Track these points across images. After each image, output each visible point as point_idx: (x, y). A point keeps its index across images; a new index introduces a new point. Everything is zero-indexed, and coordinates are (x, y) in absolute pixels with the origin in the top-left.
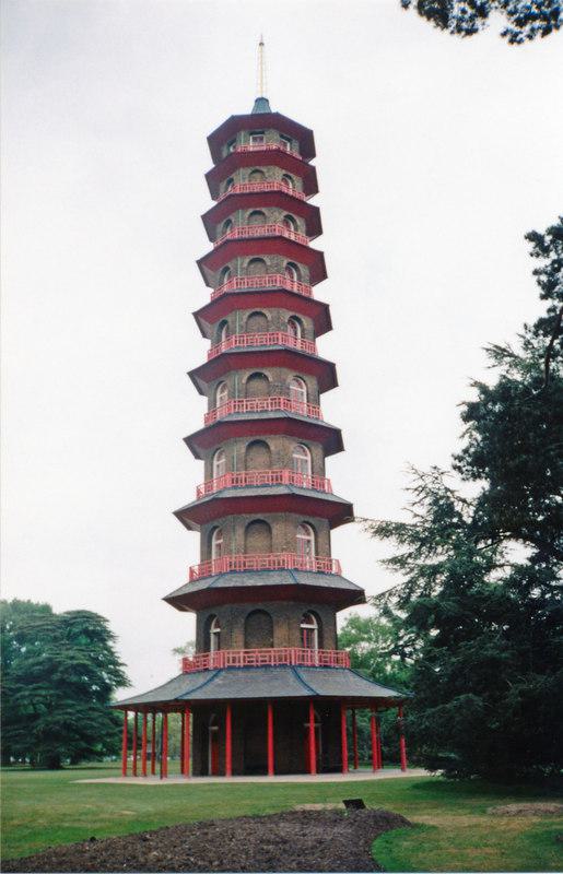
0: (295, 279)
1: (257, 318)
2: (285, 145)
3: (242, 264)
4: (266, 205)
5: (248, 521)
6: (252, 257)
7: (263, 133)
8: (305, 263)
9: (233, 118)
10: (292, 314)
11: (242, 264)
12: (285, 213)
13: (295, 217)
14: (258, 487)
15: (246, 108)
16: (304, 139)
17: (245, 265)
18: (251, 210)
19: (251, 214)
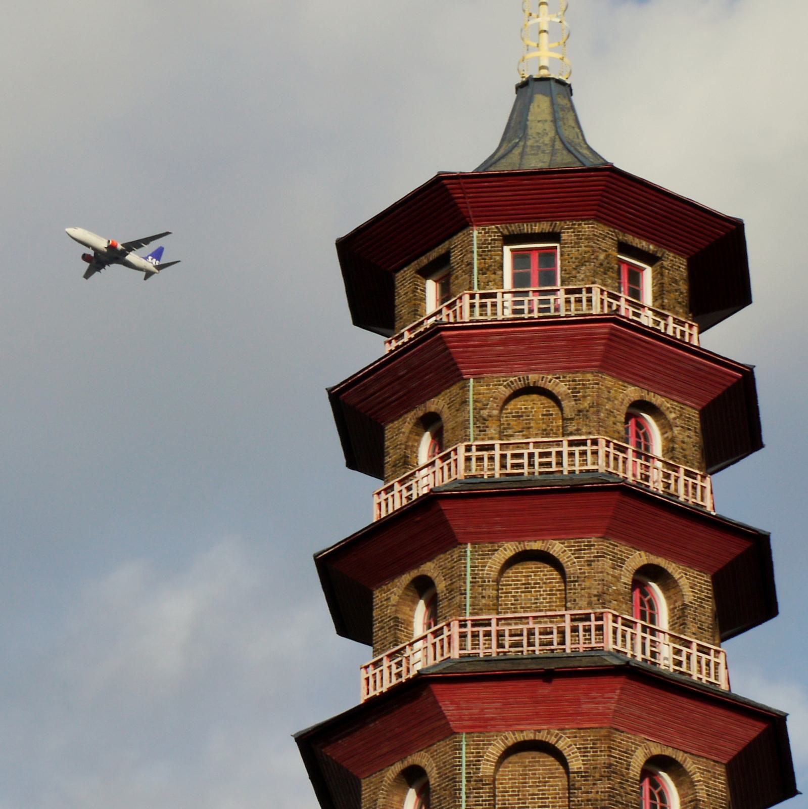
0: (663, 621)
1: (532, 566)
2: (658, 323)
3: (474, 765)
4: (561, 531)
5: (510, 742)
6: (512, 738)
7: (554, 237)
8: (690, 561)
9: (337, 633)
10: (633, 393)
11: (474, 765)
12: (639, 558)
13: (673, 568)
14: (546, 610)
15: (467, 145)
16: (713, 260)
17: (486, 769)
18: (509, 549)
19: (510, 563)
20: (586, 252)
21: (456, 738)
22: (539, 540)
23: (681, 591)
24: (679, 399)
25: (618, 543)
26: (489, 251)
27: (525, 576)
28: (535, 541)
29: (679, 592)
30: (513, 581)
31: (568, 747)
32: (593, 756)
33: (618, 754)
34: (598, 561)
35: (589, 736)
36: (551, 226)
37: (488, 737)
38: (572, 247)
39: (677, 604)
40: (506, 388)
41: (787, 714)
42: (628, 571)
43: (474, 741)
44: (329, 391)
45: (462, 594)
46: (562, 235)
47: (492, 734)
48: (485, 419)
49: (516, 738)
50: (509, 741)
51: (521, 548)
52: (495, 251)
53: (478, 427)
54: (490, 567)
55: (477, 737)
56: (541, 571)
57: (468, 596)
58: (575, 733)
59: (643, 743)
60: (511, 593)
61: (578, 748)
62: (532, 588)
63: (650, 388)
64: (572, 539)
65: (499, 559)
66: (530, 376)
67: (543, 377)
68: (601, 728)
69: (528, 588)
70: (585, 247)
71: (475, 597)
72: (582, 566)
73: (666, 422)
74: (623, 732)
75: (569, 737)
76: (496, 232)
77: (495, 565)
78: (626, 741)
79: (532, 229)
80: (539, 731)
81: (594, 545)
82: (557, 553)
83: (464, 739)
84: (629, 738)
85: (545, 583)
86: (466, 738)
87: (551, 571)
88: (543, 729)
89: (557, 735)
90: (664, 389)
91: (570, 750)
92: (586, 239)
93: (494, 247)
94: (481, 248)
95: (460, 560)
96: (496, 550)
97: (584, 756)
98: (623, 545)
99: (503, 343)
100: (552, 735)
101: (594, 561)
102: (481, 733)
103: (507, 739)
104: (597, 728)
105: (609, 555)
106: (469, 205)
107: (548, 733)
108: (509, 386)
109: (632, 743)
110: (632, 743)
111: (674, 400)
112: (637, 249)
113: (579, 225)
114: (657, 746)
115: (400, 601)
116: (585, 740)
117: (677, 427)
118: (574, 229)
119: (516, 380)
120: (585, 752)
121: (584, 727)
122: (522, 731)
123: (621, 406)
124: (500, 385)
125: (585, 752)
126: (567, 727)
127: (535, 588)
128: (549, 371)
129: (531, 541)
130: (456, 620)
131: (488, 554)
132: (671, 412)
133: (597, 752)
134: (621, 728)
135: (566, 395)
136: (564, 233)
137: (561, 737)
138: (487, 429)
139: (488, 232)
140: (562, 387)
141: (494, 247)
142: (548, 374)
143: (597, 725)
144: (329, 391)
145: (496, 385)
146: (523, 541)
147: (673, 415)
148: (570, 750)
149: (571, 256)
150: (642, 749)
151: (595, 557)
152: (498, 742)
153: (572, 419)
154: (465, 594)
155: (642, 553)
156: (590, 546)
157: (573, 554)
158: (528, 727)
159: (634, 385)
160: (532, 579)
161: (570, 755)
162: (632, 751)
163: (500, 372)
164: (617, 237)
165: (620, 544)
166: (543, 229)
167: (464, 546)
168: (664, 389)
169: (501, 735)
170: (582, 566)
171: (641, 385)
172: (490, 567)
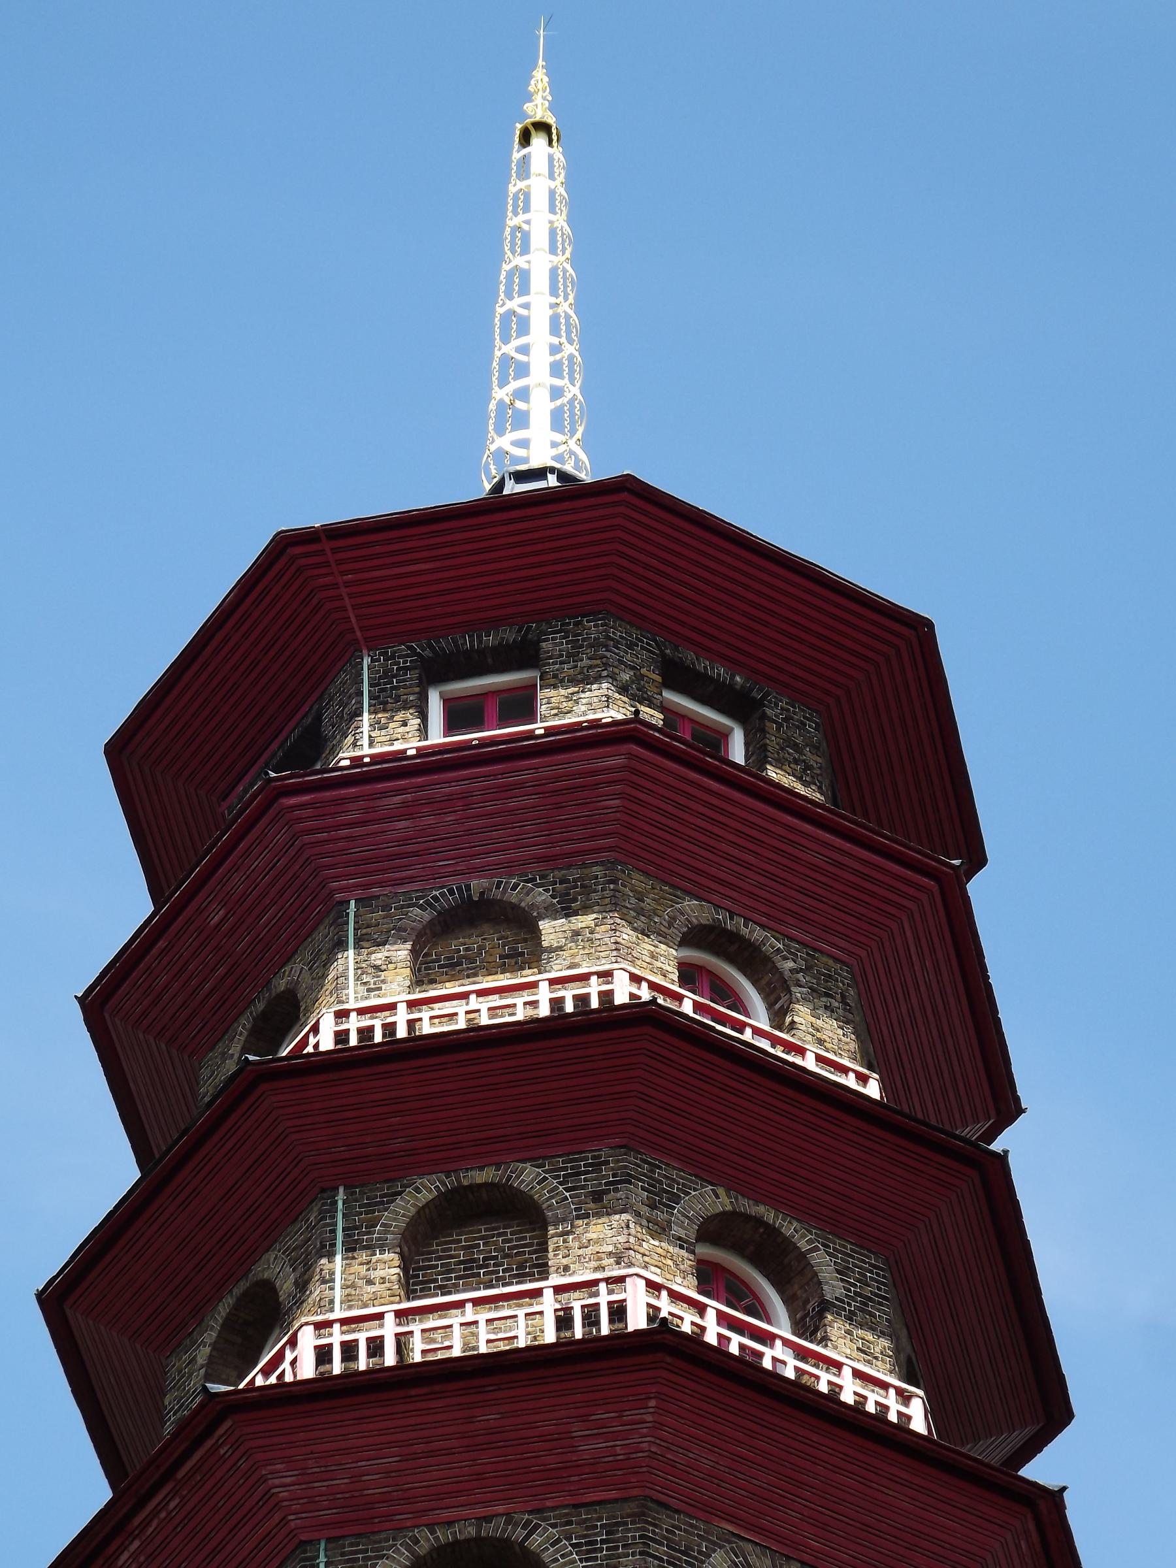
18: (424, 1190)
20: (590, 667)
21: (305, 1552)
22: (491, 1165)
23: (816, 1274)
24: (807, 938)
25: (661, 1162)
26: (393, 688)
27: (464, 1248)
28: (481, 1168)
29: (811, 1279)
30: (439, 1258)
31: (553, 1545)
32: (608, 1557)
33: (666, 1553)
34: (616, 1190)
35: (600, 1519)
36: (519, 631)
37: (376, 1542)
38: (562, 663)
39: (810, 1307)
40: (424, 910)
41: (1064, 1489)
42: (687, 1217)
43: (343, 1554)
44: (81, 1000)
45: (324, 1282)
46: (544, 645)
47: (383, 1535)
48: (378, 968)
49: (437, 1539)
50: (422, 1546)
51: (450, 1182)
52: (405, 687)
53: (365, 983)
54: (383, 1225)
55: (351, 1545)
56: (499, 1235)
57: (338, 1284)
58: (566, 1515)
59: (730, 1542)
60: (436, 1281)
61: (573, 1546)
62: (481, 1267)
63: (735, 908)
64: (559, 1156)
65: (404, 1208)
66: (474, 883)
67: (499, 883)
68: (625, 1500)
69: (471, 1268)
70: (589, 659)
71: (353, 1286)
72: (580, 1203)
73: (777, 976)
74: (677, 1511)
75: (554, 1526)
76: (407, 656)
77: (395, 1220)
78: (685, 1531)
79: (480, 642)
80: (488, 1519)
81: (607, 1163)
82: (528, 1185)
83: (322, 1554)
84: (691, 1525)
85: (506, 1256)
86: (326, 1550)
87: (521, 1232)
88: (496, 1515)
89: (528, 1522)
90: (764, 909)
91: (557, 1551)
92: (590, 646)
93: (405, 681)
94: (379, 684)
95: (324, 1218)
96: (400, 1193)
97: (587, 1560)
98: (674, 1168)
99: (407, 812)
100: (516, 1525)
101: (607, 1192)
102: (359, 1535)
103: (417, 1542)
104: (616, 1501)
105: (640, 1180)
106: (344, 591)
107: (507, 1523)
108: (430, 905)
109: (699, 1536)
110: (699, 1536)
111: (791, 939)
112: (704, 677)
113: (577, 624)
114: (765, 1555)
115: (214, 1353)
116: (587, 1528)
117: (800, 986)
118: (567, 632)
119: (443, 894)
120: (589, 1552)
121: (588, 1500)
122: (450, 1523)
123: (669, 928)
124: (409, 906)
125: (589, 1552)
126: (549, 1503)
127: (487, 1266)
128: (510, 868)
129: (472, 1169)
130: (307, 1324)
131: (382, 1203)
132: (785, 958)
133: (617, 1548)
134: (673, 1502)
135: (546, 908)
136: (547, 640)
137: (537, 1526)
138: (384, 986)
139: (393, 657)
140: (540, 894)
141: (405, 681)
142: (511, 876)
143: (613, 1494)
144: (81, 1000)
145: (402, 907)
146: (455, 1171)
147: (790, 964)
148: (557, 1551)
149: (561, 676)
150: (727, 1553)
151: (608, 1184)
152: (397, 1551)
153: (560, 948)
154: (333, 1281)
155: (721, 1191)
156: (597, 1166)
157: (561, 1183)
158: (466, 1512)
159: (698, 898)
160: (480, 1252)
161: (557, 1560)
162: (700, 1552)
163: (412, 879)
164: (660, 649)
165: (667, 1164)
166: (503, 639)
167: (329, 1193)
168: (764, 909)
169: (405, 1536)
170: (580, 1203)
171: (715, 898)
172: (383, 1225)
